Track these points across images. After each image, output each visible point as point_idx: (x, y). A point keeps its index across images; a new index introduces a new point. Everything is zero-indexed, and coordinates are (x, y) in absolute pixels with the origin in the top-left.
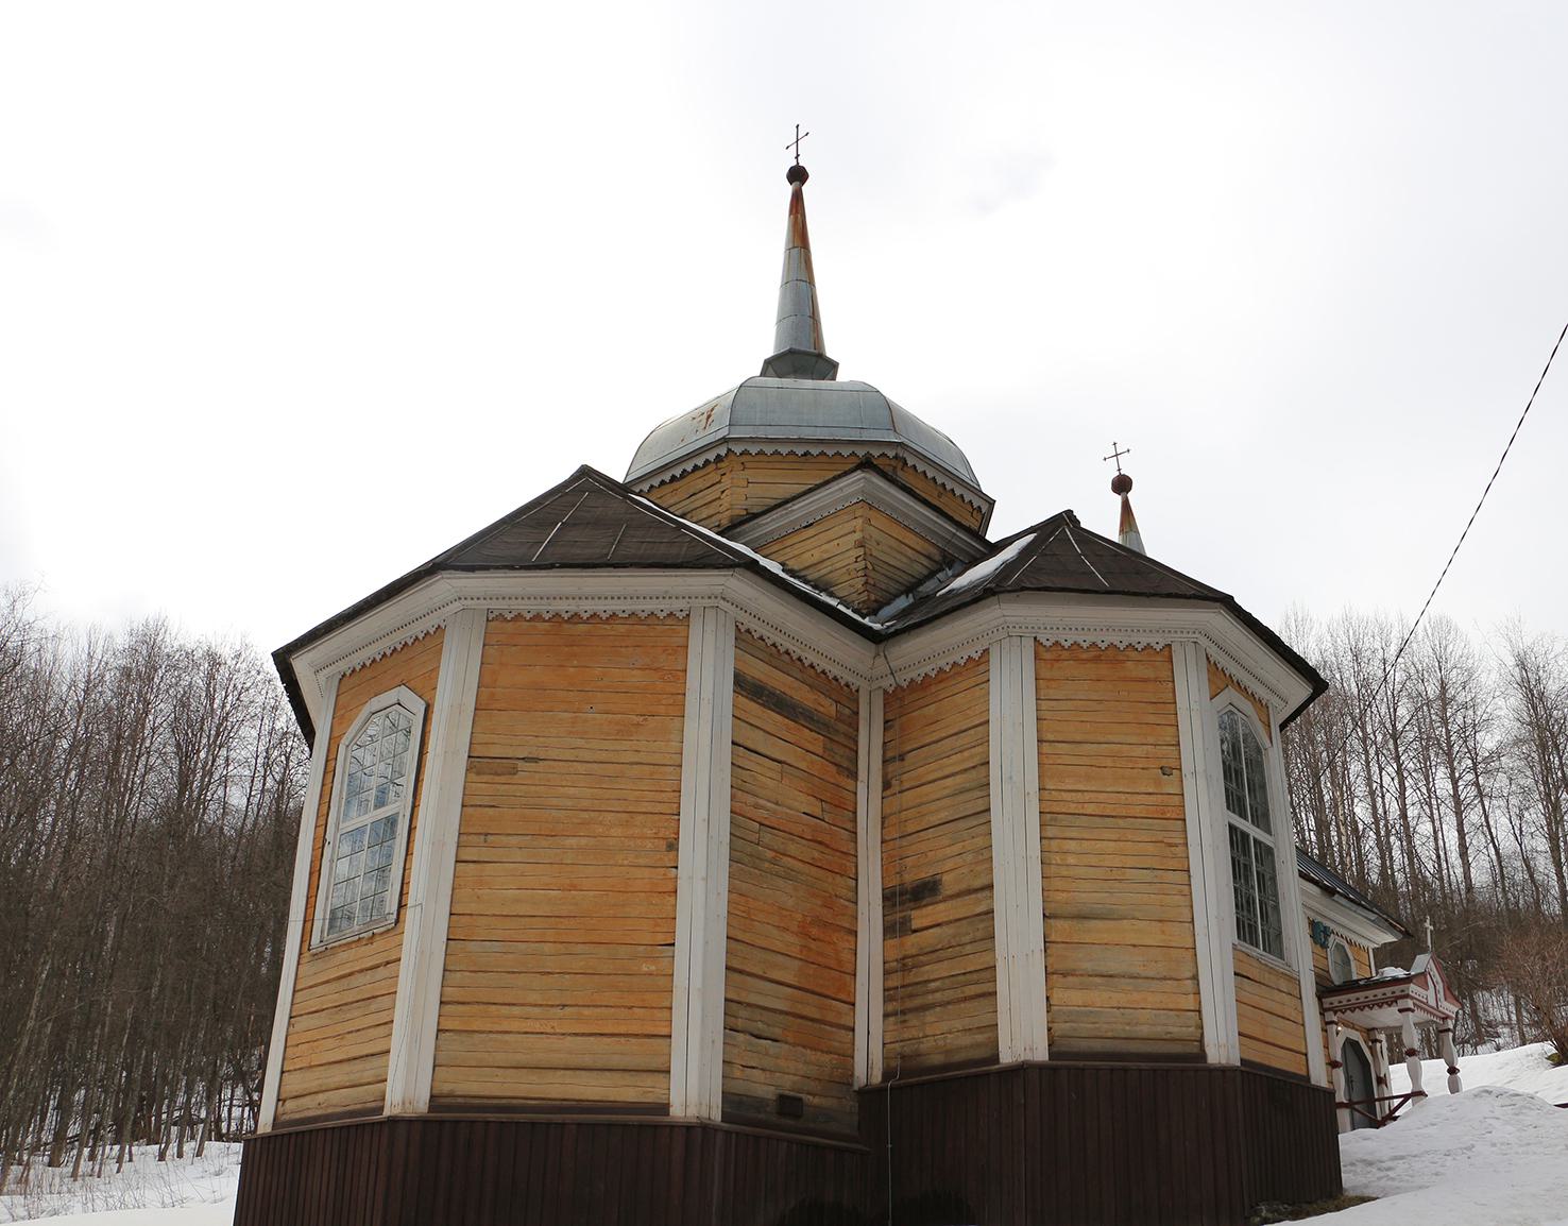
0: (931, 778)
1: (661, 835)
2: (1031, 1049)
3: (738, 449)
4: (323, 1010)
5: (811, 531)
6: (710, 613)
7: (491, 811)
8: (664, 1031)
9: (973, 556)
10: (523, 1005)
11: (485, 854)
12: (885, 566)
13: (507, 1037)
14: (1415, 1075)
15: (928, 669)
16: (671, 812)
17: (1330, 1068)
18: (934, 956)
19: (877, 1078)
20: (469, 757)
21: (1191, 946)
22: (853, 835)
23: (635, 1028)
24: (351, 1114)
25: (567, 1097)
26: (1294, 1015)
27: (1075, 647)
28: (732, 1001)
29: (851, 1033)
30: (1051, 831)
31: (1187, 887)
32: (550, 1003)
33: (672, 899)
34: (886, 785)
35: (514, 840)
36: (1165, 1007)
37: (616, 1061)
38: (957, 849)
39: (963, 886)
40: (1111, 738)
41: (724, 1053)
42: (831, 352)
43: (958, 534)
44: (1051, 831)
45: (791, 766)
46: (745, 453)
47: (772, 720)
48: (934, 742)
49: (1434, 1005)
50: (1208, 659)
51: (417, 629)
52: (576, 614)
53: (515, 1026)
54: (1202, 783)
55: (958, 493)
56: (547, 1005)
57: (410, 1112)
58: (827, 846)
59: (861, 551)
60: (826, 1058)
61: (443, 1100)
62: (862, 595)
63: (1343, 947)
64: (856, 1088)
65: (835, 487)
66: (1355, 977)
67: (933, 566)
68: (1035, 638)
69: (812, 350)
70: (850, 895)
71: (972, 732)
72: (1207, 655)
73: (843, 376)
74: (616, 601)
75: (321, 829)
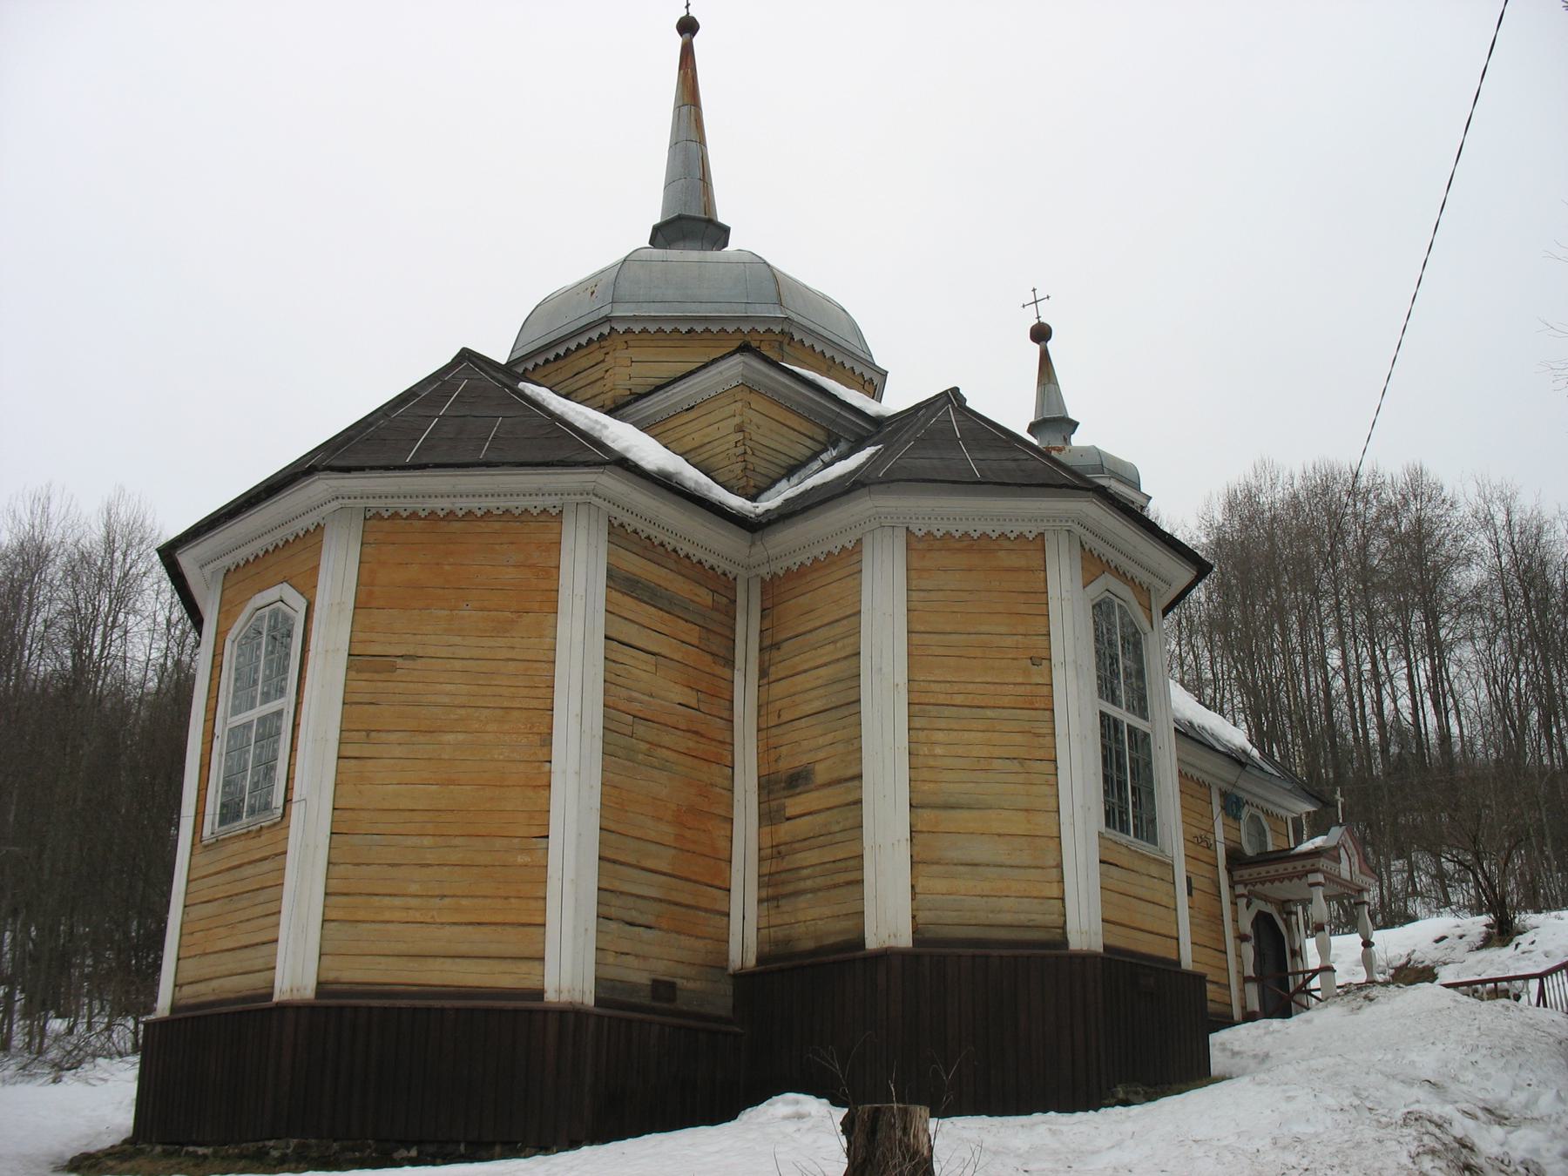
0: (806, 667)
1: (535, 730)
2: (895, 936)
3: (621, 328)
4: (216, 900)
5: (692, 415)
6: (583, 510)
7: (371, 708)
8: (539, 920)
9: (858, 434)
10: (403, 895)
11: (367, 751)
12: (766, 450)
13: (390, 926)
14: (1324, 950)
15: (804, 557)
16: (545, 707)
17: (1238, 941)
18: (806, 843)
19: (751, 961)
20: (349, 655)
21: (1055, 834)
22: (730, 724)
23: (511, 918)
24: (244, 1000)
25: (446, 983)
26: (1165, 900)
27: (948, 536)
28: (606, 890)
29: (726, 919)
30: (918, 723)
31: (1054, 777)
32: (430, 894)
33: (546, 793)
34: (763, 673)
35: (393, 737)
36: (1027, 894)
37: (493, 949)
38: (829, 738)
39: (835, 775)
40: (983, 628)
41: (597, 941)
42: (722, 218)
43: (842, 413)
44: (918, 723)
45: (666, 658)
46: (628, 331)
47: (647, 613)
48: (810, 631)
49: (1349, 878)
50: (1082, 546)
51: (299, 526)
52: (451, 511)
53: (398, 915)
54: (1071, 673)
55: (848, 365)
56: (427, 896)
57: (297, 996)
58: (702, 736)
59: (740, 436)
60: (699, 944)
61: (330, 987)
62: (741, 481)
63: (1258, 818)
64: (731, 971)
65: (713, 370)
66: (1270, 848)
67: (817, 447)
68: (907, 528)
69: (703, 216)
70: (726, 783)
71: (845, 622)
72: (1081, 542)
73: (734, 243)
74: (489, 499)
75: (211, 723)
